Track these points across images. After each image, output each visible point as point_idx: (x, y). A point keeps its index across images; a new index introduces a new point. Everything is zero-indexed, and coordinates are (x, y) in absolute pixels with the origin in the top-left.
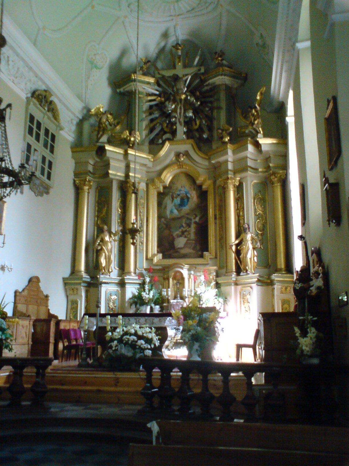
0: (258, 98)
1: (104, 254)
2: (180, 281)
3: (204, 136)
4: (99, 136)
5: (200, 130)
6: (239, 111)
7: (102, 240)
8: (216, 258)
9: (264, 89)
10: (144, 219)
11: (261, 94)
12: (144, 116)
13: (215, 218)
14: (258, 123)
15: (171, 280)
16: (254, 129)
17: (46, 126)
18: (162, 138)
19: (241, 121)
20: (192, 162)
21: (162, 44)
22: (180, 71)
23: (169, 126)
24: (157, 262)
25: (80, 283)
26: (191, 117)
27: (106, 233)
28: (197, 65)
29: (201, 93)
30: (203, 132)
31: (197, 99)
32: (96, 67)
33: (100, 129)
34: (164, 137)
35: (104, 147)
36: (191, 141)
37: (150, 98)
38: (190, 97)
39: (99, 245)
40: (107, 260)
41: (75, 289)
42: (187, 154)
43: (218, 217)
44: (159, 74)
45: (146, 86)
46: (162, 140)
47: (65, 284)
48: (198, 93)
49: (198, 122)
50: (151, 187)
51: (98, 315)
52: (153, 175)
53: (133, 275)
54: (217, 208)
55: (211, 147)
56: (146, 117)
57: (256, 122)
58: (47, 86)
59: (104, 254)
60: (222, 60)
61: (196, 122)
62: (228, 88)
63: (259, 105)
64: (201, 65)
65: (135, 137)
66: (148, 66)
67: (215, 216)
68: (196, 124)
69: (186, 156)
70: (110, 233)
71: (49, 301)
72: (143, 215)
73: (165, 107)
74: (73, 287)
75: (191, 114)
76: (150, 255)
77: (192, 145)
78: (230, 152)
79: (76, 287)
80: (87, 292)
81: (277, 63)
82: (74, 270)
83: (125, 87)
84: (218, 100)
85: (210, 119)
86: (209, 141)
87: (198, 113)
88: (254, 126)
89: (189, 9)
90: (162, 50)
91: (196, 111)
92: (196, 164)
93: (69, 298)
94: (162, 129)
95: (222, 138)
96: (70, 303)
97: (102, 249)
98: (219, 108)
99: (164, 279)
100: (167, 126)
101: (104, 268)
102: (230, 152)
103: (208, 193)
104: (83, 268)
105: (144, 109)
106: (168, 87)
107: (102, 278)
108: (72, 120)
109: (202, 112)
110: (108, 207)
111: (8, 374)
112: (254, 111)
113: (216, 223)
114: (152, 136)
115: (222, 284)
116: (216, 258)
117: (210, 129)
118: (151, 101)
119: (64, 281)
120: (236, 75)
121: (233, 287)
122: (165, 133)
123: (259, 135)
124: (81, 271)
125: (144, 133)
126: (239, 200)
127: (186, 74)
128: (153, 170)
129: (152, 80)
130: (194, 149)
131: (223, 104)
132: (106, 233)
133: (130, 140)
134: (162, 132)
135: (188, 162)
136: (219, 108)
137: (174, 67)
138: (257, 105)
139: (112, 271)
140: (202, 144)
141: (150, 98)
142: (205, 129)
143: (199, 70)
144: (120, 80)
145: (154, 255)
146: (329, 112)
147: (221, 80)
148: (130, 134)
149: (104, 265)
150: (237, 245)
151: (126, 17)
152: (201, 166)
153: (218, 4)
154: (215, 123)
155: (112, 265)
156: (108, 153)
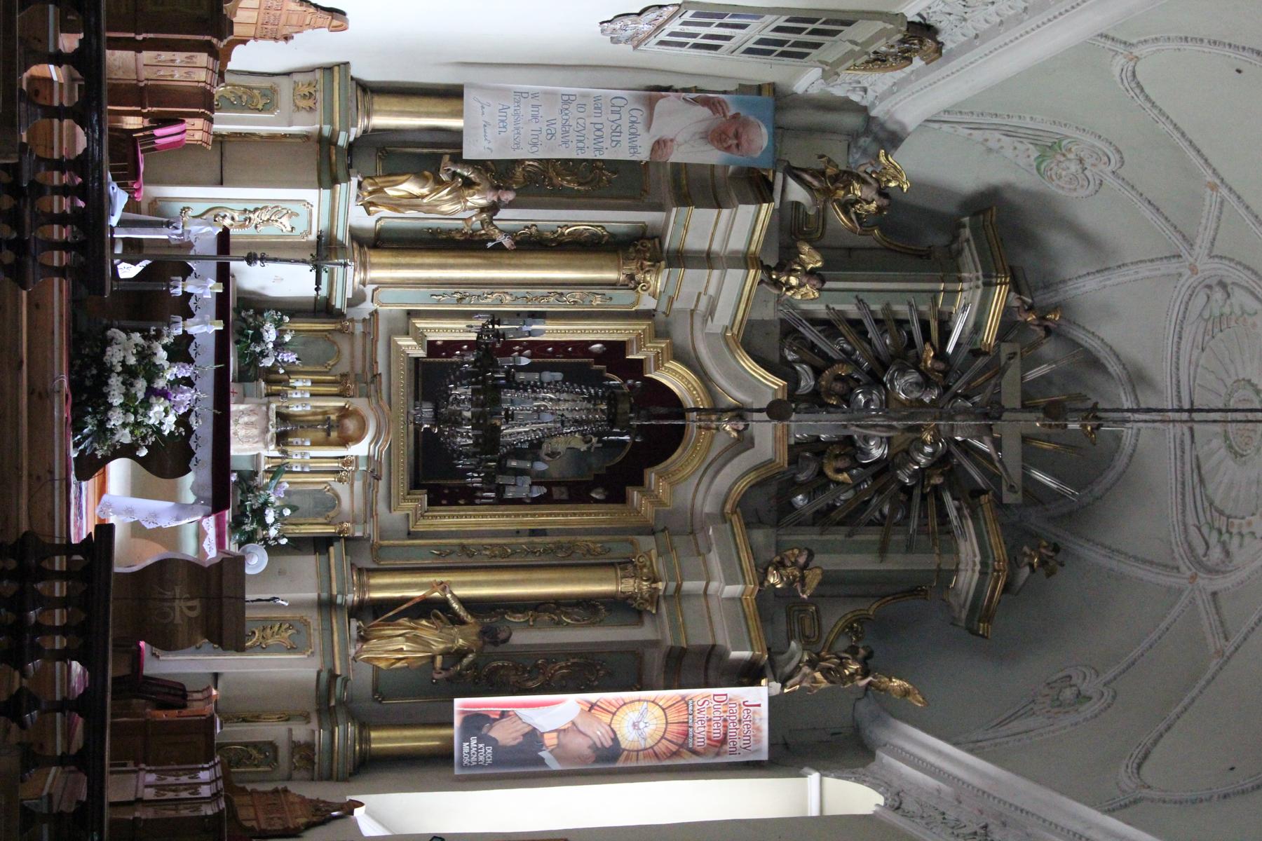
0: (896, 683)
1: (425, 191)
2: (334, 434)
3: (800, 497)
4: (808, 178)
5: (820, 483)
6: (871, 608)
7: (468, 184)
8: (410, 535)
9: (917, 701)
10: (540, 305)
11: (906, 693)
12: (876, 307)
13: (533, 533)
14: (815, 680)
15: (339, 403)
16: (798, 668)
17: (827, 44)
18: (802, 361)
19: (834, 618)
20: (719, 455)
21: (1114, 367)
22: (1012, 428)
23: (838, 386)
24: (400, 346)
25: (332, 123)
26: (867, 454)
27: (491, 197)
28: (1027, 478)
29: (936, 488)
30: (810, 496)
31: (921, 475)
32: (1041, 158)
33: (831, 181)
34: (804, 369)
35: (769, 199)
36: (783, 459)
37: (934, 325)
38: (932, 454)
39: (455, 175)
40: (405, 201)
41: (311, 103)
42: (744, 442)
43: (536, 540)
44: (1012, 356)
45: (973, 309)
46: (794, 361)
47: (328, 69)
48: (937, 480)
49: (844, 477)
50: (642, 326)
51: (223, 259)
52: (680, 334)
53: (357, 279)
54: (564, 539)
55: (760, 523)
56: (872, 312)
57: (818, 675)
58: (953, 55)
59: (425, 191)
60: (1031, 565)
61: (847, 470)
62: (945, 577)
63: (870, 683)
64: (1025, 491)
65: (801, 285)
66: (1040, 317)
67: (542, 533)
68: (839, 471)
69: (738, 440)
70: (493, 208)
71: (272, 42)
72: (548, 304)
73: (903, 371)
74: (319, 96)
75: (877, 453)
76: (420, 324)
77: (771, 461)
78: (734, 590)
79: (319, 106)
80: (306, 137)
81: (968, 767)
82: (370, 91)
83: (972, 242)
84: (909, 548)
85: (853, 518)
86: (782, 514)
87: (875, 477)
88: (806, 670)
89: (1205, 469)
90: (1094, 363)
91: (884, 468)
92: (720, 461)
93: (284, 80)
94: (830, 362)
95: (780, 565)
96: (265, 83)
97: (440, 183)
98: (883, 550)
99: (343, 375)
100: (838, 378)
101: (381, 190)
102: (734, 590)
103: (619, 506)
104: (379, 121)
105: (896, 308)
106: (964, 379)
107: (348, 190)
108: (865, 90)
109: (880, 491)
110: (578, 195)
111: (55, 78)
112: (855, 667)
113: (518, 533)
114: (811, 333)
115: (324, 558)
116: (410, 535)
117: (823, 518)
118: (925, 325)
119: (339, 65)
120: (980, 612)
121: (313, 596)
122: (817, 372)
123: (776, 686)
124: (368, 114)
125: (820, 309)
126: (587, 607)
127: (1003, 444)
128: (699, 335)
129: (989, 335)
130: (755, 468)
131: (896, 563)
132: (491, 197)
133: (792, 272)
134: (819, 362)
135: (720, 444)
136: (883, 550)
137: (1026, 407)
138: (870, 679)
139: (369, 213)
140: (773, 489)
141: (934, 325)
142: (822, 501)
143: (1011, 488)
144: (999, 231)
145: (419, 336)
146: (1030, 722)
147: (969, 561)
148: (812, 273)
149: (390, 192)
150: (443, 605)
151: (1193, 270)
152: (700, 496)
153: (1200, 563)
154: (837, 536)
155: (385, 212)
156: (752, 208)
